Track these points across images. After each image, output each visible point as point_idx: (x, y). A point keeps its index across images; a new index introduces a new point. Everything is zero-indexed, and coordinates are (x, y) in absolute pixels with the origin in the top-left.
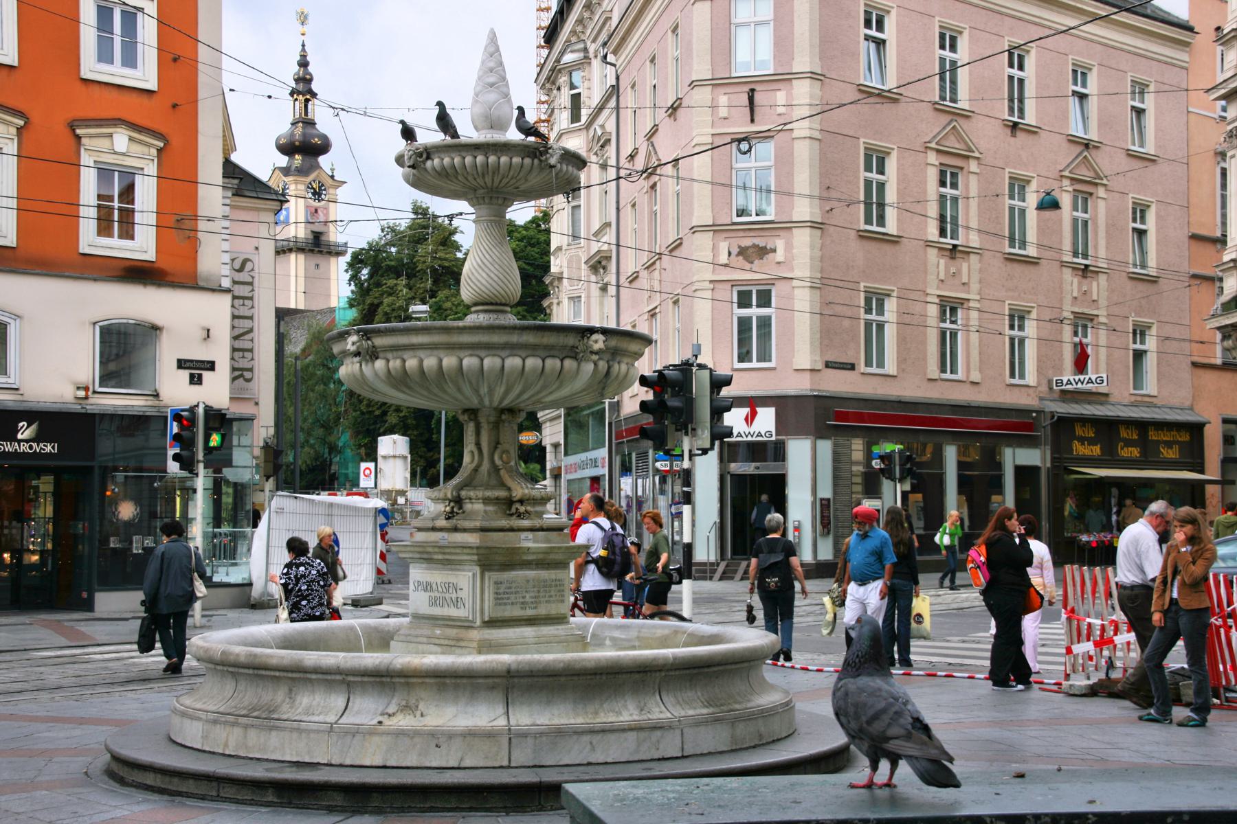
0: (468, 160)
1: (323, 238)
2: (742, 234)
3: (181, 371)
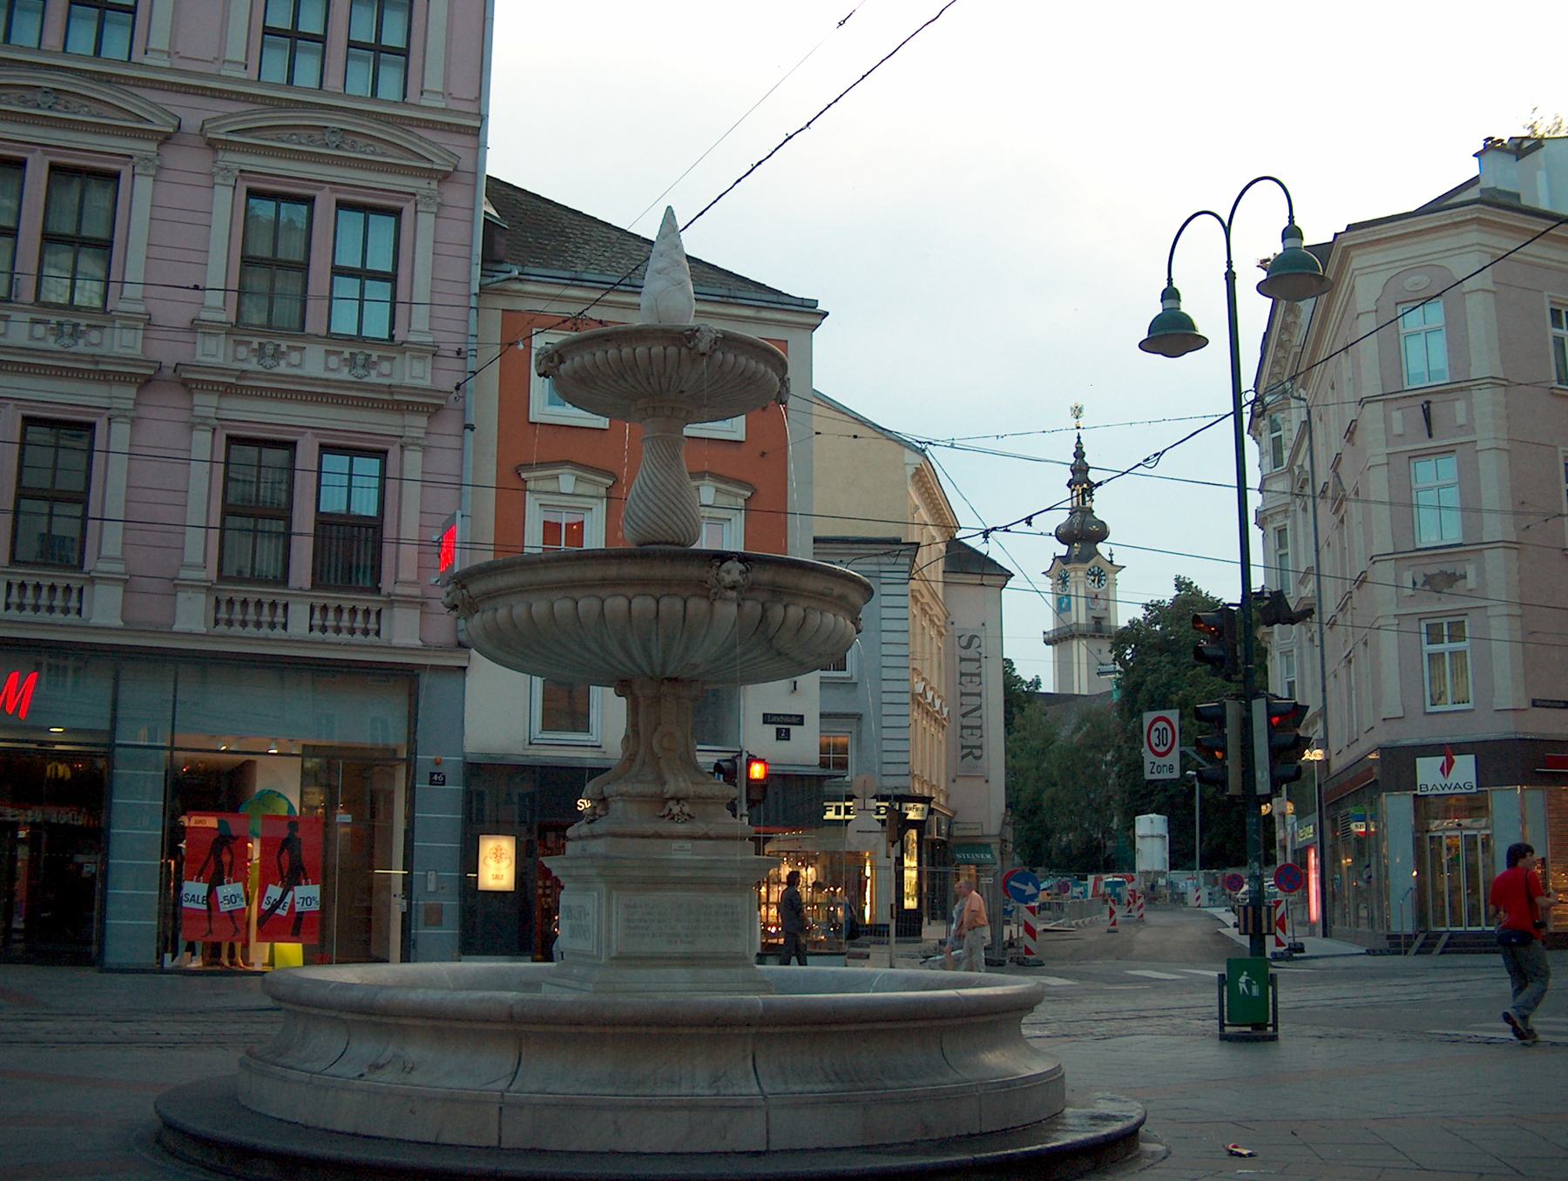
0: (599, 354)
1: (1104, 623)
2: (1427, 560)
3: (767, 726)
